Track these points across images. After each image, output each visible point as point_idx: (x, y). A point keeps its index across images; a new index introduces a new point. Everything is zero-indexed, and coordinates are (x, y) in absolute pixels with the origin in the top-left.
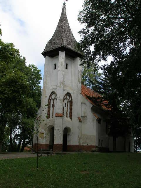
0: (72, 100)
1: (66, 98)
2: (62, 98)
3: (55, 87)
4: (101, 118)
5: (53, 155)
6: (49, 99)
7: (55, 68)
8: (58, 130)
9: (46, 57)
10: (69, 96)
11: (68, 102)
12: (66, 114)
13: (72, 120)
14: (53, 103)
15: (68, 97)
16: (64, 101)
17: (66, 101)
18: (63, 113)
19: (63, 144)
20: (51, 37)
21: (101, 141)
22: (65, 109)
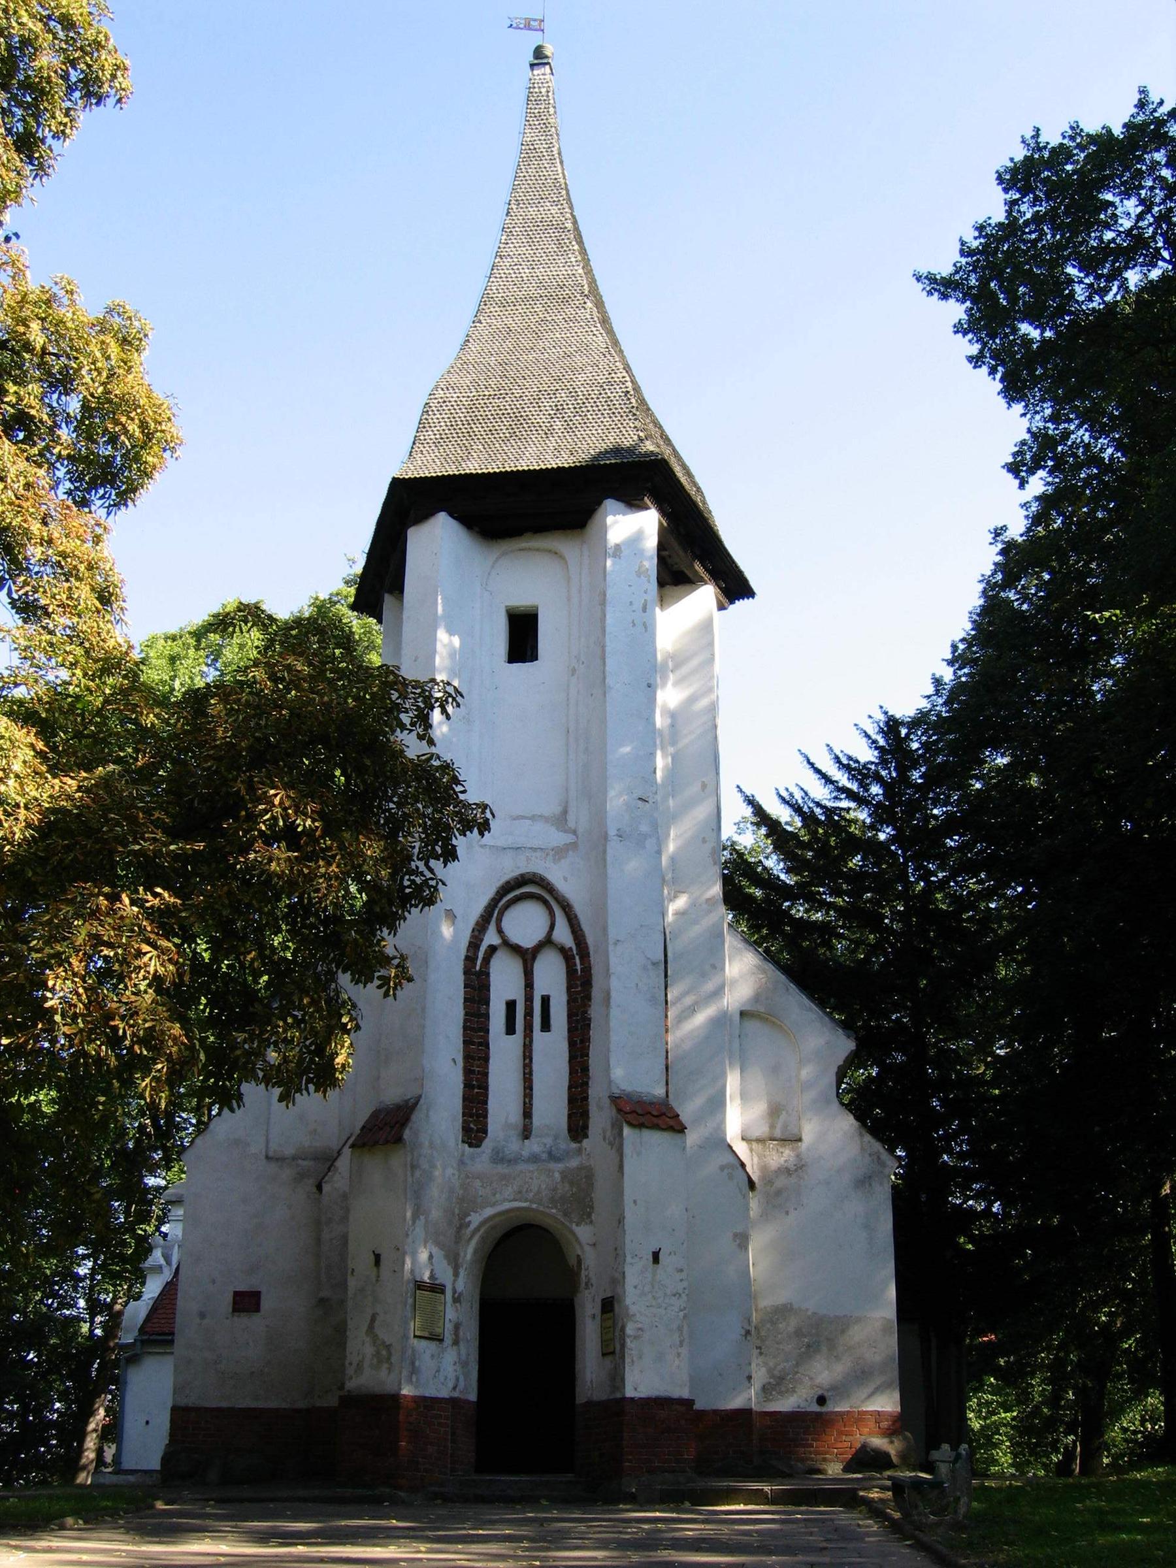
6: (474, 945)
8: (656, 1257)
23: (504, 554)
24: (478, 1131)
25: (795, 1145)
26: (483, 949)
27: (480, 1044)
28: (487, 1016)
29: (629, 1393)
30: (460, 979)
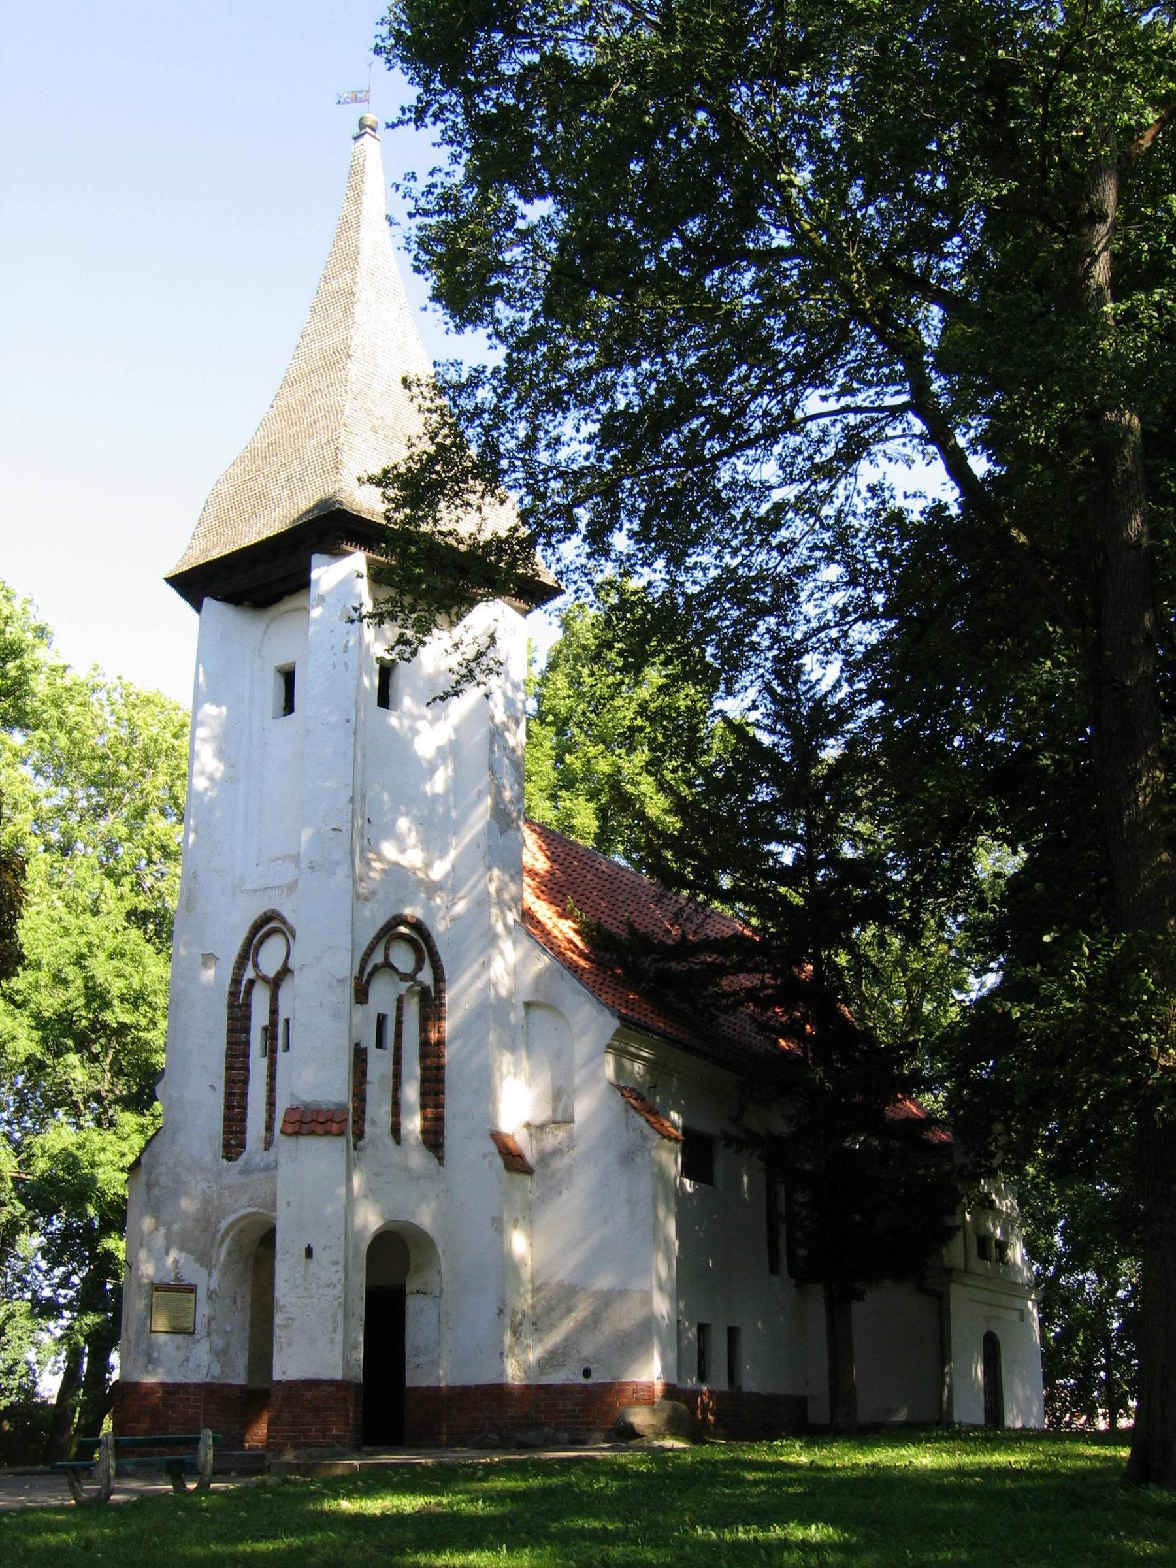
0: (439, 977)
1: (388, 964)
2: (344, 965)
3: (287, 872)
5: (1042, 1457)
6: (236, 981)
7: (289, 707)
8: (309, 1252)
9: (208, 603)
10: (417, 950)
11: (400, 1001)
12: (387, 1108)
13: (441, 1159)
14: (274, 1012)
15: (403, 958)
16: (361, 995)
17: (383, 994)
18: (360, 1095)
19: (358, 1374)
21: (719, 1344)
22: (379, 1064)
23: (272, 620)
24: (237, 1146)
25: (567, 1126)
26: (244, 982)
27: (240, 1069)
28: (247, 1043)
29: (277, 1376)
30: (224, 1012)
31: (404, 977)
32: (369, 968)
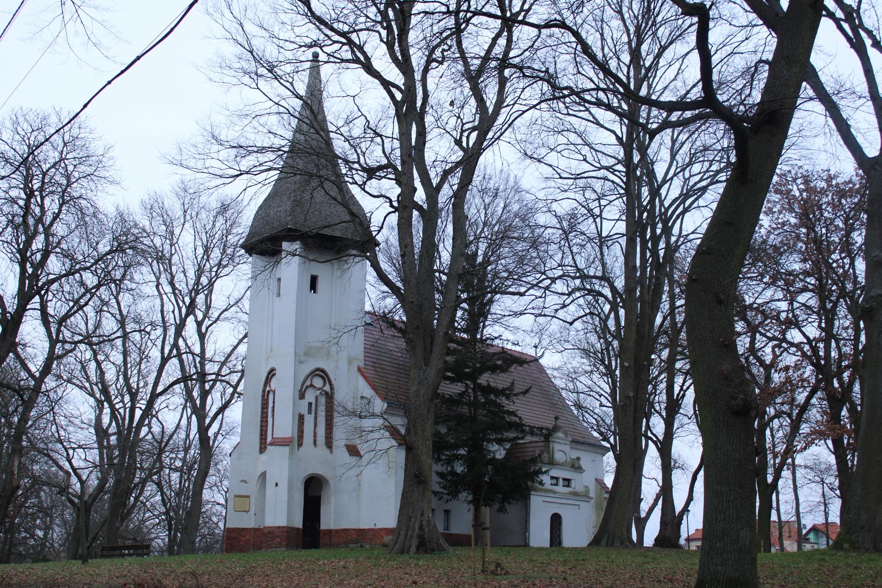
0: (332, 388)
1: (312, 385)
4: (592, 494)
6: (264, 391)
11: (317, 397)
15: (318, 382)
16: (302, 396)
17: (310, 396)
20: (699, 59)
31: (319, 389)
32: (304, 387)
